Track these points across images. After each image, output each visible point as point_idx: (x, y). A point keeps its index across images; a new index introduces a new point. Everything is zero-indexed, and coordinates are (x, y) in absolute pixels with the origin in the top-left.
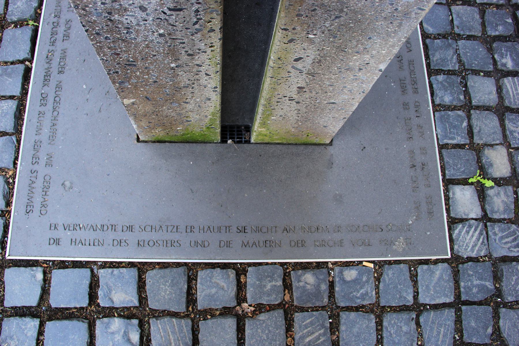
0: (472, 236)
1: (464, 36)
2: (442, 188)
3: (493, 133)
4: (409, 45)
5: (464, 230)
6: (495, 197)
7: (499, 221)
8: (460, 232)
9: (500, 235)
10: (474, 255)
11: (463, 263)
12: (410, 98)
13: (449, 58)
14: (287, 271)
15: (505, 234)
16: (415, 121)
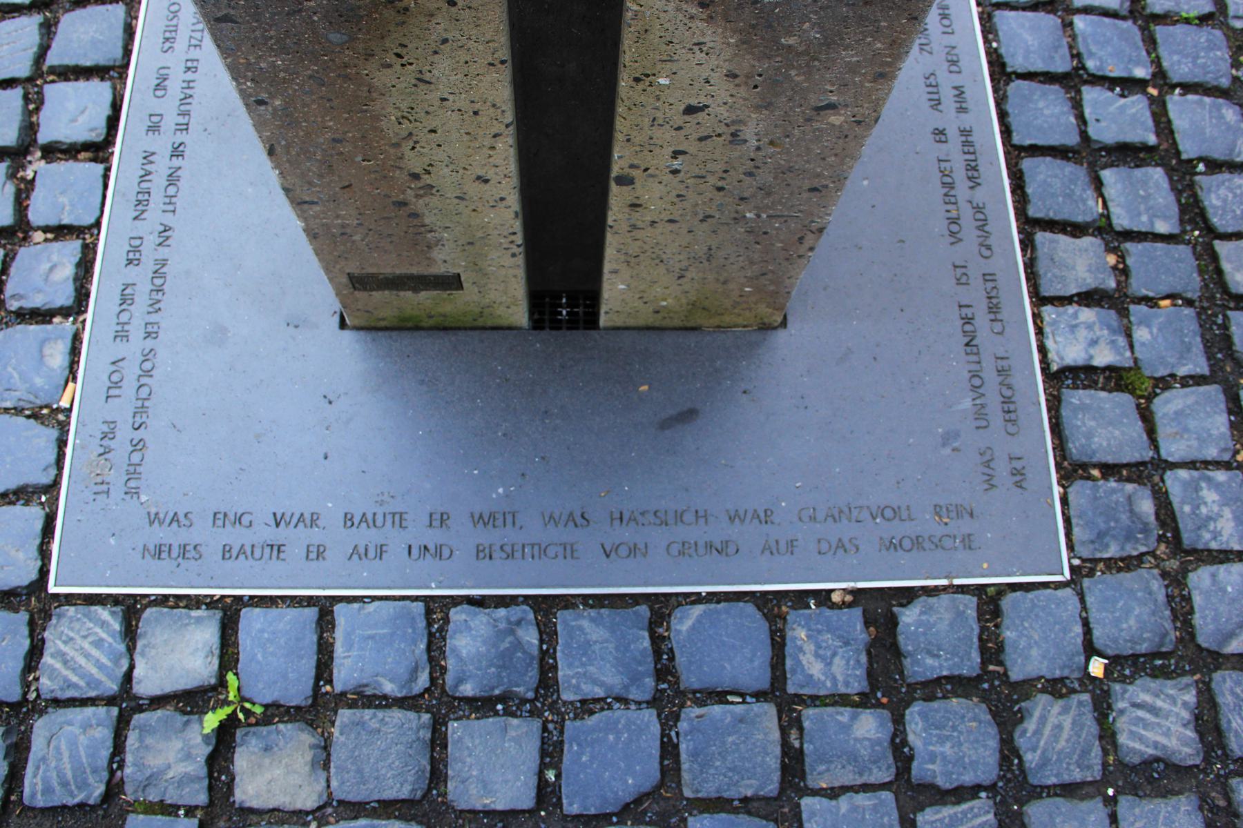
0: (87, 656)
1: (673, 734)
2: (218, 592)
3: (359, 771)
4: (623, 551)
5: (104, 635)
6: (179, 745)
7: (118, 748)
8: (103, 624)
9: (83, 740)
10: (47, 659)
11: (32, 624)
12: (463, 537)
13: (591, 669)
14: (82, 234)
15: (82, 753)
16: (396, 541)
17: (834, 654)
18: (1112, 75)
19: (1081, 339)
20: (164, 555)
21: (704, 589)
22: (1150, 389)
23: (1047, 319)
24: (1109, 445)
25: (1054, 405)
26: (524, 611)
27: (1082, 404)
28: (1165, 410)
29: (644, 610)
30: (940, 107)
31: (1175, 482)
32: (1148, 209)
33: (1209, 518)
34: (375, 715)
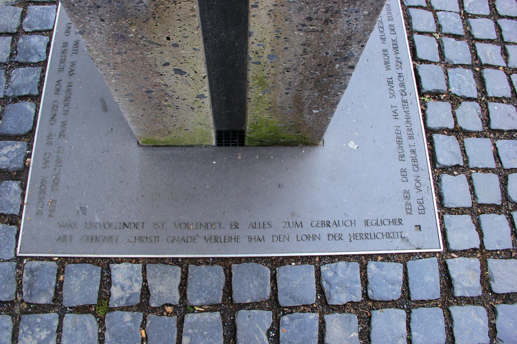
17: (8, 157)
18: (281, 331)
19: (125, 282)
20: (384, 37)
21: (40, 114)
22: (99, 315)
23: (135, 265)
24: (71, 284)
25: (93, 261)
26: (44, 57)
27: (93, 276)
28: (87, 320)
29: (36, 93)
30: (251, 227)
31: (53, 317)
32: (195, 333)
33: (33, 332)
34: (18, 16)
